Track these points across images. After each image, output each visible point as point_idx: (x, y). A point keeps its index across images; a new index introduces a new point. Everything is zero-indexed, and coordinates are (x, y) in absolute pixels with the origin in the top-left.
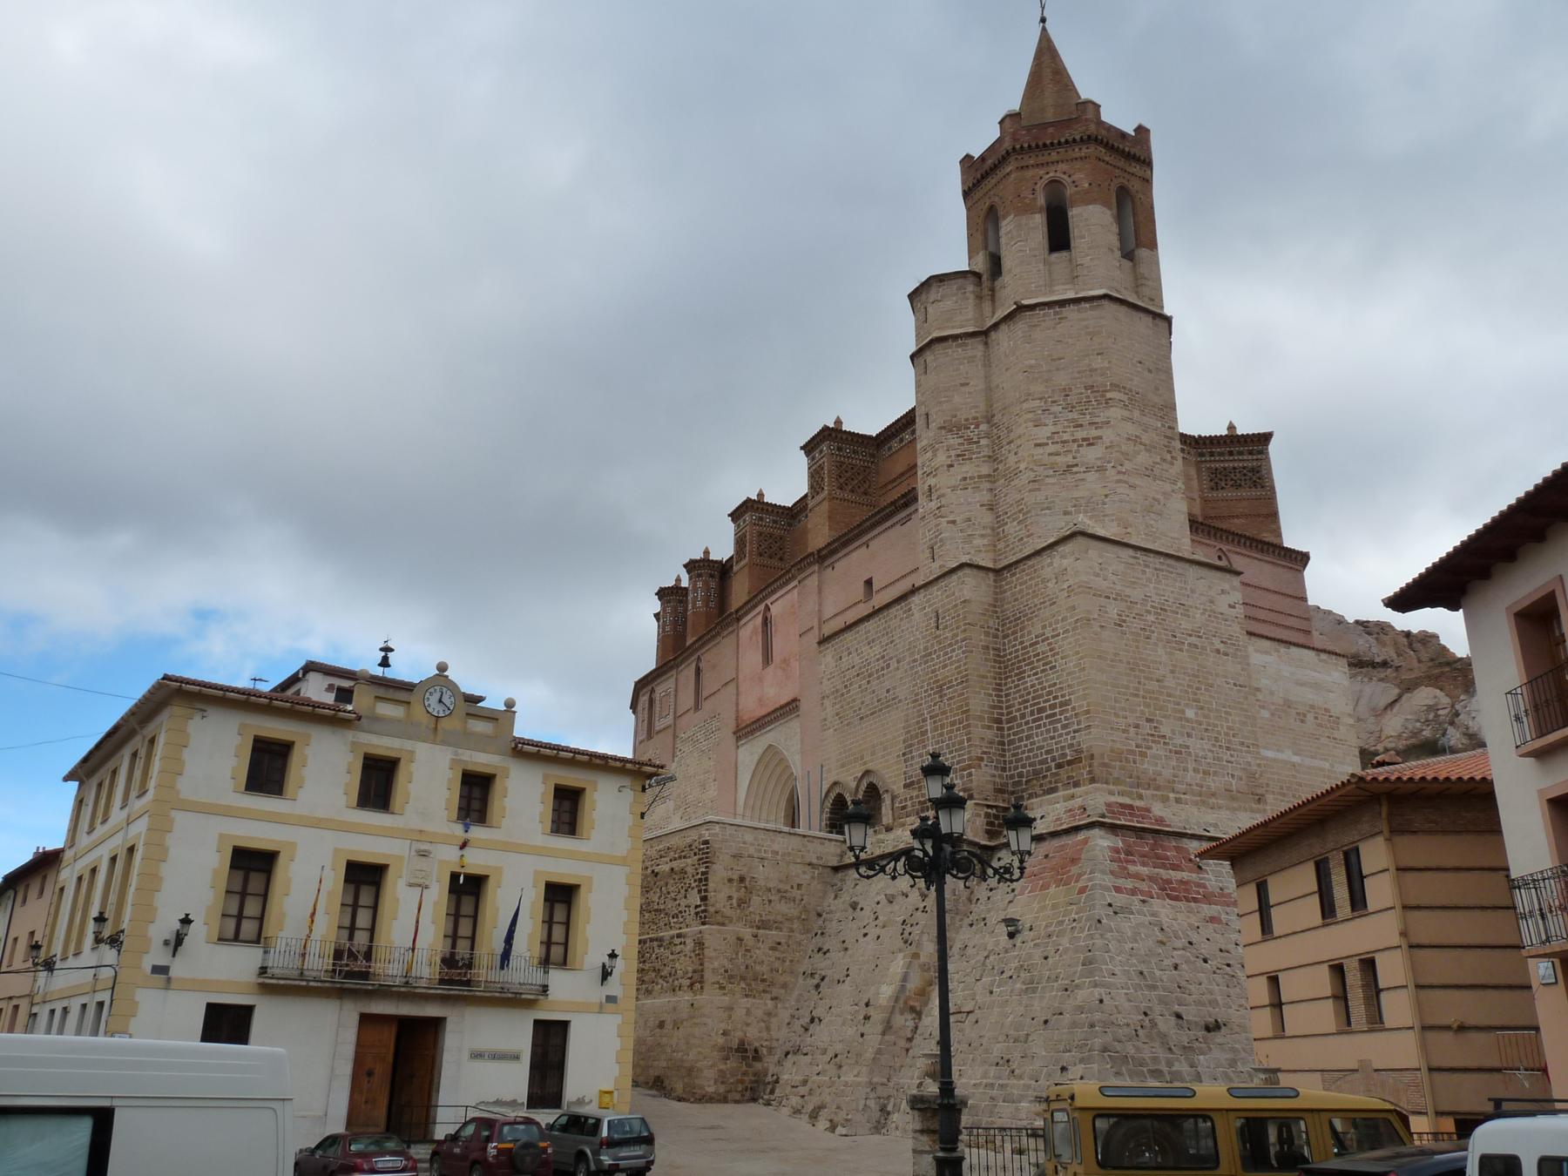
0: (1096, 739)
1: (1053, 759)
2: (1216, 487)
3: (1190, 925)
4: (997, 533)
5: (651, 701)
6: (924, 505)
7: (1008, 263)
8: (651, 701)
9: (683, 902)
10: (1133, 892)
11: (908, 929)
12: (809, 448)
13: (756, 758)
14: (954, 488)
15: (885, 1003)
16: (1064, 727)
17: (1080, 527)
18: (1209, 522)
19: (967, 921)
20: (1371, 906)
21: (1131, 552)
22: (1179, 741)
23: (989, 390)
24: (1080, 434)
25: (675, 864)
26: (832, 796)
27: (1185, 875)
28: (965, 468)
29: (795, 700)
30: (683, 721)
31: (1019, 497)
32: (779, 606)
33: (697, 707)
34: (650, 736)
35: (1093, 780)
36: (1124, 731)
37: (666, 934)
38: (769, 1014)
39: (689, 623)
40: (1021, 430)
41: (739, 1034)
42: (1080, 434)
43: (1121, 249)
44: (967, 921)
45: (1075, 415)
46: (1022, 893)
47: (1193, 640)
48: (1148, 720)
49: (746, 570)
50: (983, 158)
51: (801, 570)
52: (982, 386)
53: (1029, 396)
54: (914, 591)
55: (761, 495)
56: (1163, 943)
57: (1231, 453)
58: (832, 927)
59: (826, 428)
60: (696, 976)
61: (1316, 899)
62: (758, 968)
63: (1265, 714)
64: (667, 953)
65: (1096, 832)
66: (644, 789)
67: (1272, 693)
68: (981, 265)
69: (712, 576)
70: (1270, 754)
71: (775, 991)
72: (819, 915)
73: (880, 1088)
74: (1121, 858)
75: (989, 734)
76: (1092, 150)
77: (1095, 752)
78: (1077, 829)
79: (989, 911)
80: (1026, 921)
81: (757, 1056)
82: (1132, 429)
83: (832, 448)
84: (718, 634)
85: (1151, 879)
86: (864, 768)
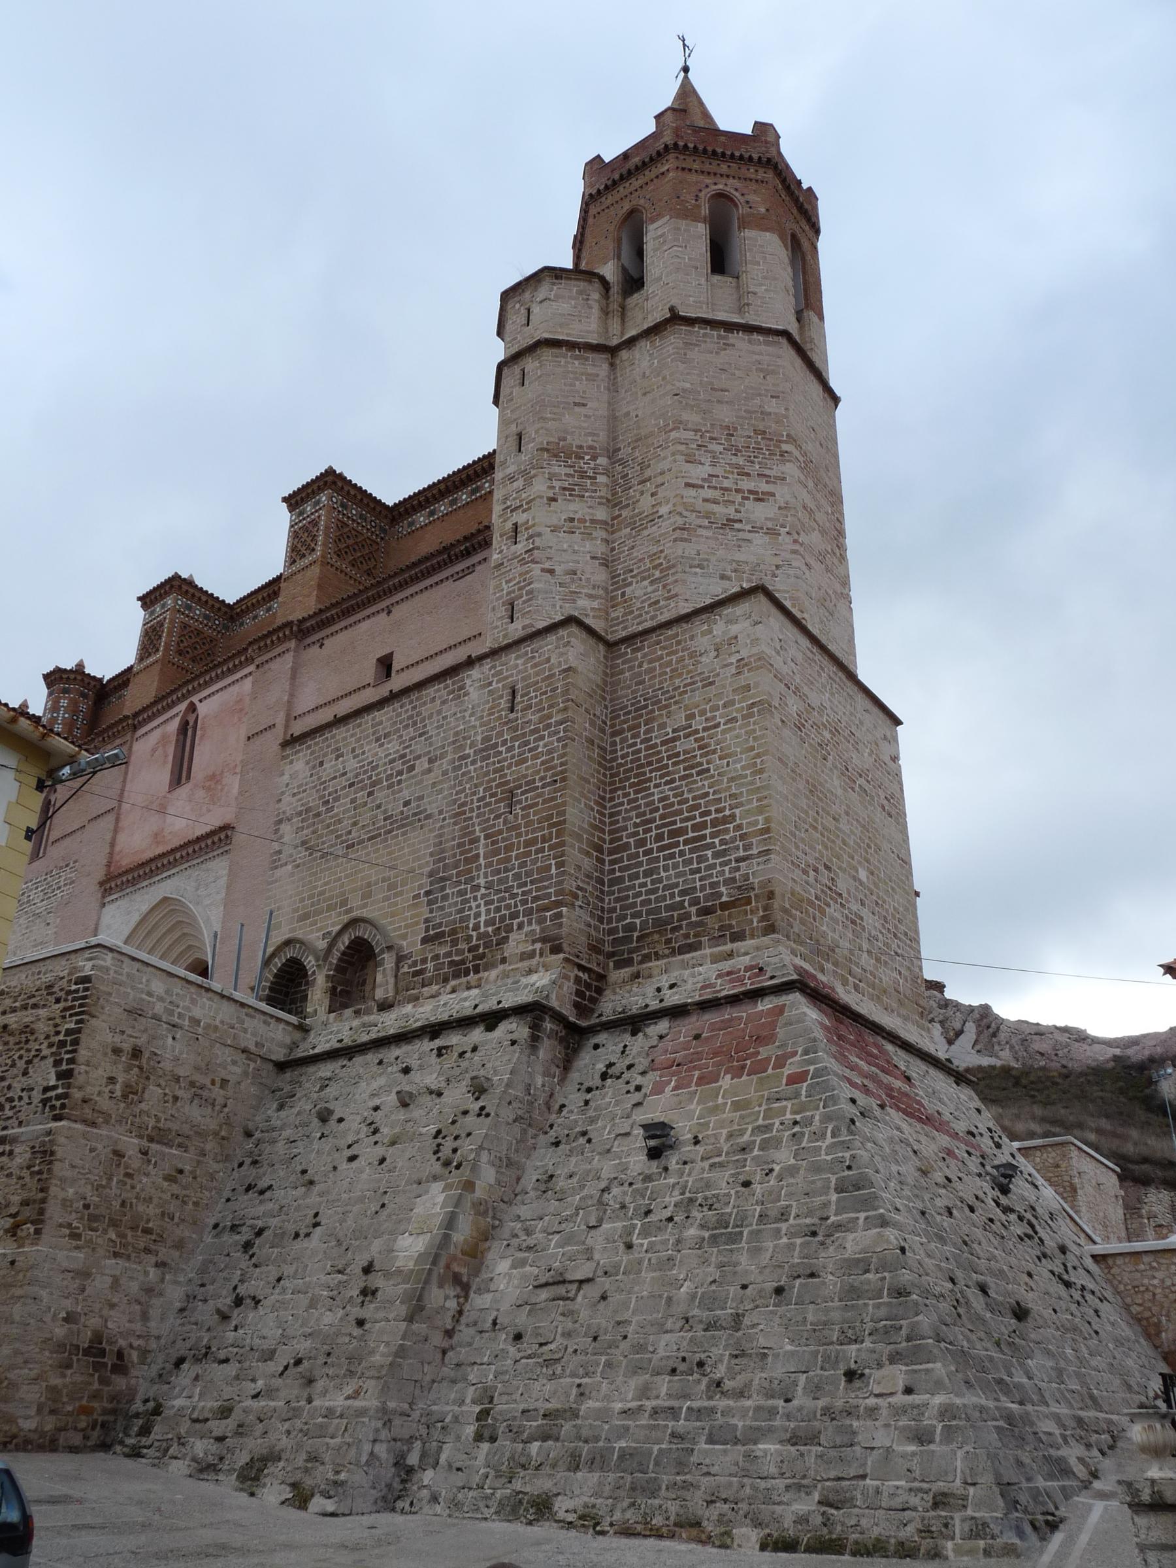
0: (780, 872)
6: (500, 550)
11: (449, 1144)
12: (294, 501)
13: (136, 918)
14: (555, 529)
15: (411, 1265)
16: (717, 855)
24: (746, 484)
29: (225, 828)
35: (771, 929)
38: (149, 1291)
40: (664, 465)
41: (94, 1322)
42: (746, 484)
49: (157, 667)
52: (603, 412)
53: (679, 424)
54: (470, 662)
60: (27, 1212)
62: (141, 1208)
69: (83, 695)
71: (164, 1253)
72: (249, 1134)
73: (397, 1421)
77: (778, 891)
78: (757, 994)
79: (592, 1121)
80: (683, 1129)
81: (121, 1366)
82: (804, 495)
86: (346, 918)
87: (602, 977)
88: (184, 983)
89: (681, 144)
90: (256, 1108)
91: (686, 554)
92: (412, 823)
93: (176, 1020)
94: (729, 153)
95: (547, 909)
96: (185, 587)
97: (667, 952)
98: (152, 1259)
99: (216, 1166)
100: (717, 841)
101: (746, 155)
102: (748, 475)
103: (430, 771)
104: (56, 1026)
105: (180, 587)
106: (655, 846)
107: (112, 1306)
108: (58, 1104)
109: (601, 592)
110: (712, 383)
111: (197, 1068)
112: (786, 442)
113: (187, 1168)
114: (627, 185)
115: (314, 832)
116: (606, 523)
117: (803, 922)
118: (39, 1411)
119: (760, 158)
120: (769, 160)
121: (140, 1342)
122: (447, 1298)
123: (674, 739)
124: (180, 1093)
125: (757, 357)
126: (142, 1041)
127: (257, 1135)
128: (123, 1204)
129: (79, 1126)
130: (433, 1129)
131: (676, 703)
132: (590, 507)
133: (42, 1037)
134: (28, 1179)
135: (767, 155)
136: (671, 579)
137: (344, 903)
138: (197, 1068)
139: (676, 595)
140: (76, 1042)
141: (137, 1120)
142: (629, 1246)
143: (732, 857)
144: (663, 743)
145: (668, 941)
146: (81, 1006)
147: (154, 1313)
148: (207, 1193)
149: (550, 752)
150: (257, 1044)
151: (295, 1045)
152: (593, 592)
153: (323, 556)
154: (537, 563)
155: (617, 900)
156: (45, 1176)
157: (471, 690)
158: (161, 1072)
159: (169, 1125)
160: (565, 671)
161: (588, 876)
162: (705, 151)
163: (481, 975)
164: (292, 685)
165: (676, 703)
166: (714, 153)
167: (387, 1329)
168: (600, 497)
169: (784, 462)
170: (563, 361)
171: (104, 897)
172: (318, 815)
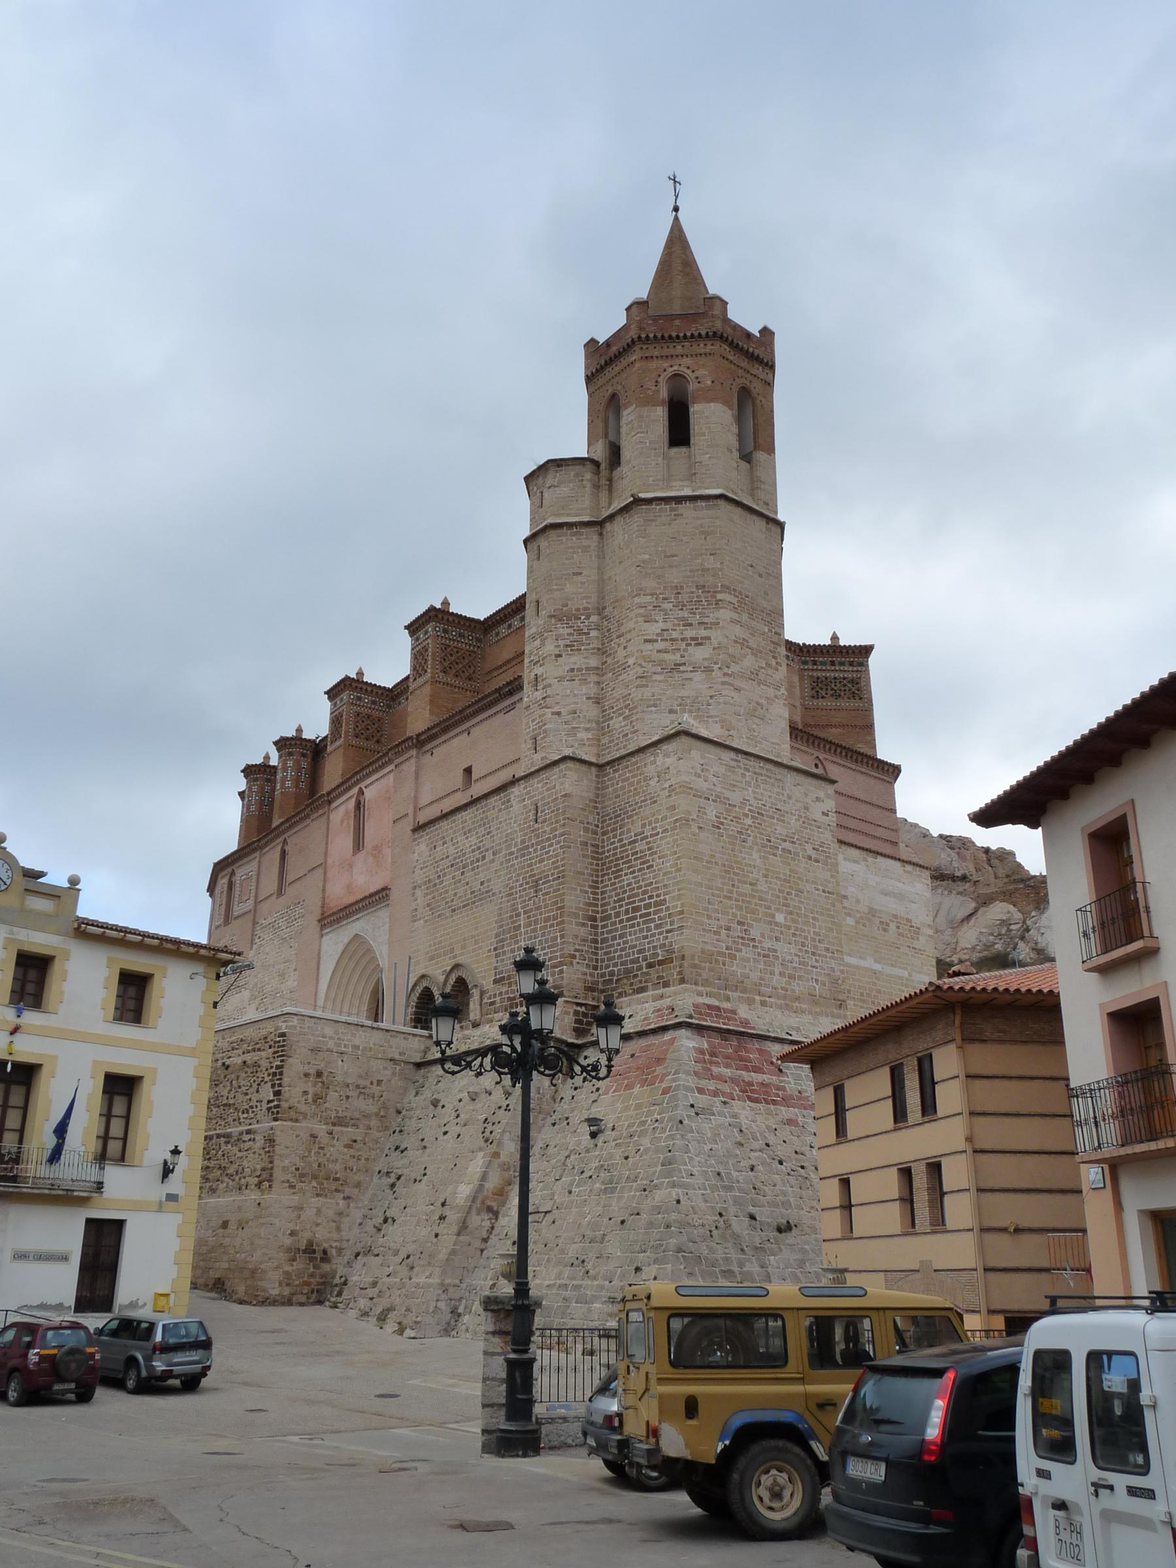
1: (645, 959)
3: (768, 1127)
4: (601, 727)
5: (231, 885)
6: (529, 694)
7: (626, 453)
8: (231, 885)
9: (255, 1097)
10: (715, 1093)
13: (341, 948)
14: (561, 679)
16: (657, 927)
17: (684, 727)
19: (550, 1120)
21: (732, 755)
22: (768, 944)
23: (601, 582)
25: (247, 1057)
26: (419, 989)
28: (573, 659)
29: (385, 889)
30: (264, 907)
32: (374, 789)
33: (280, 892)
34: (227, 921)
35: (682, 981)
36: (717, 933)
37: (234, 1130)
38: (340, 1214)
39: (277, 805)
40: (631, 625)
41: (307, 1235)
42: (690, 633)
43: (739, 450)
44: (550, 1120)
46: (606, 1093)
47: (787, 845)
48: (739, 923)
49: (341, 750)
50: (608, 344)
53: (641, 591)
54: (514, 782)
58: (412, 1124)
65: (683, 1032)
66: (218, 977)
67: (858, 901)
68: (600, 453)
69: (304, 755)
71: (348, 1191)
72: (399, 1112)
73: (451, 1290)
74: (706, 1059)
76: (717, 347)
78: (664, 1029)
79: (573, 1110)
80: (609, 1120)
81: (325, 1257)
82: (738, 631)
84: (307, 816)
86: (453, 962)
89: (643, 336)
90: (404, 1094)
94: (682, 335)
95: (556, 967)
96: (354, 685)
98: (341, 1195)
99: (379, 1135)
101: (696, 334)
102: (690, 625)
103: (493, 861)
107: (318, 1225)
109: (594, 725)
110: (664, 552)
111: (360, 1077)
112: (720, 592)
113: (359, 1138)
116: (597, 668)
118: (280, 1284)
120: (715, 333)
121: (337, 1244)
122: (483, 1220)
123: (635, 842)
125: (700, 522)
126: (322, 1066)
127: (404, 1112)
128: (319, 1166)
130: (483, 1117)
135: (714, 329)
136: (635, 717)
137: (452, 950)
138: (360, 1077)
140: (281, 1074)
142: (570, 1192)
144: (630, 843)
145: (631, 984)
147: (344, 1226)
149: (556, 856)
150: (400, 1054)
155: (606, 953)
157: (514, 803)
159: (345, 1114)
160: (565, 796)
161: (584, 940)
162: (663, 337)
164: (416, 783)
166: (670, 337)
167: (448, 1239)
169: (718, 609)
170: (564, 539)
172: (435, 885)
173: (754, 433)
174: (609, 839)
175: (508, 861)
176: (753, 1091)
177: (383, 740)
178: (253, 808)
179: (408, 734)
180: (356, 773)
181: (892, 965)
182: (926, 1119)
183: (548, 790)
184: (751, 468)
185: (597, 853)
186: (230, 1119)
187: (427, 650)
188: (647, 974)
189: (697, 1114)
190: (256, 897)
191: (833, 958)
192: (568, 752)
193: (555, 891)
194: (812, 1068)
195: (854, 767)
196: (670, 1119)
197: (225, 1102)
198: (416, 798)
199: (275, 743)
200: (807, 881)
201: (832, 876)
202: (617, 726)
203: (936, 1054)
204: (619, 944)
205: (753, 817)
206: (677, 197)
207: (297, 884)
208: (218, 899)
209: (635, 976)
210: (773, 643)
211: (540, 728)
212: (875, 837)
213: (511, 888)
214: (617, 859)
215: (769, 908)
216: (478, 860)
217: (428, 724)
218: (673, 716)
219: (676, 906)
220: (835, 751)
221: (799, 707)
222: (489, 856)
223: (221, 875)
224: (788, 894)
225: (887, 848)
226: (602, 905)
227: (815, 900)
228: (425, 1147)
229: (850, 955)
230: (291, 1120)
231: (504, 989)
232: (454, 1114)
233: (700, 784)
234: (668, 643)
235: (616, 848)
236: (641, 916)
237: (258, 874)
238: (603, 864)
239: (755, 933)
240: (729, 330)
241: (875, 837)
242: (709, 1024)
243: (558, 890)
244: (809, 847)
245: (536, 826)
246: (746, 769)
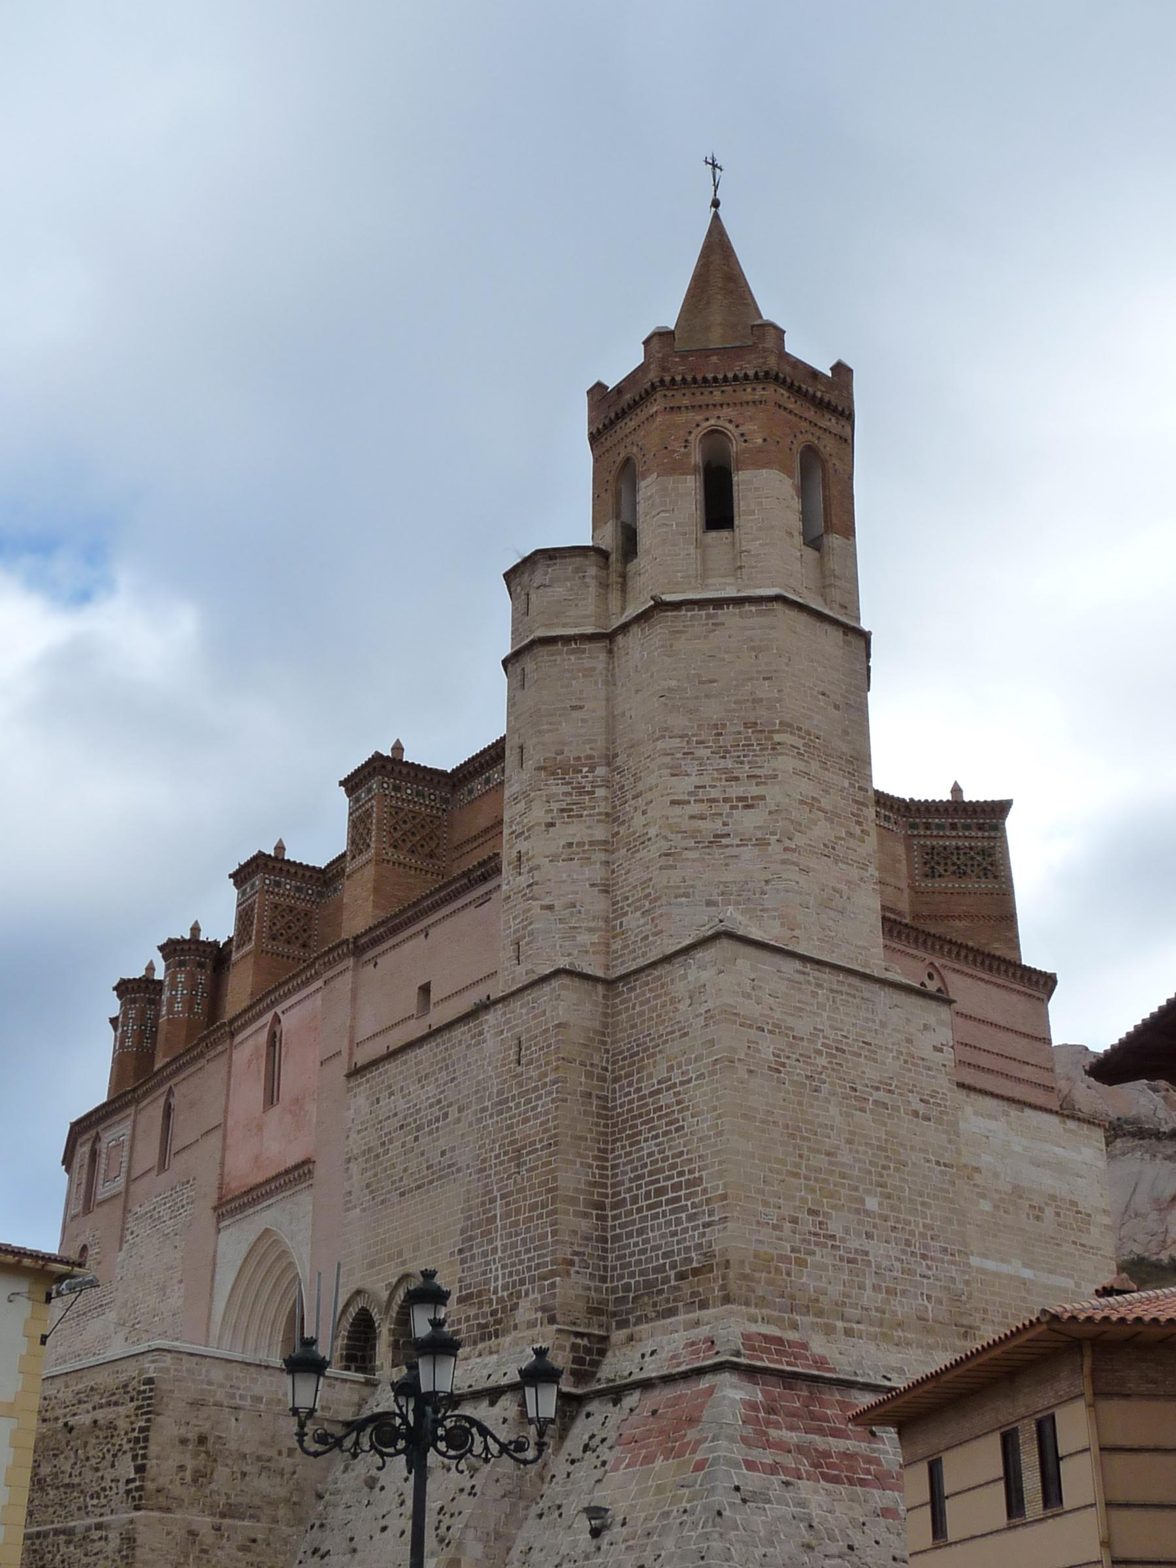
0: (736, 1239)
1: (673, 1266)
2: (931, 874)
3: (852, 1521)
4: (611, 926)
5: (94, 1154)
6: (509, 880)
7: (646, 540)
8: (94, 1154)
9: (109, 1474)
10: (773, 1469)
13: (244, 1249)
14: (553, 859)
16: (691, 1218)
17: (728, 926)
18: (916, 924)
19: (535, 1510)
20: (1068, 1502)
21: (798, 965)
22: (854, 1243)
23: (611, 721)
25: (100, 1415)
26: (353, 1311)
27: (850, 1445)
28: (572, 829)
29: (307, 1162)
30: (139, 1188)
31: (646, 876)
32: (296, 1014)
33: (162, 1166)
34: (87, 1209)
35: (727, 1300)
36: (775, 1227)
37: (79, 1523)
39: (161, 1038)
40: (652, 780)
42: (735, 791)
43: (804, 534)
44: (535, 1510)
45: (729, 763)
46: (615, 1469)
47: (881, 1095)
48: (811, 1212)
49: (251, 959)
50: (619, 389)
51: (329, 965)
53: (666, 732)
55: (280, 848)
56: (809, 1547)
57: (954, 827)
58: (337, 1515)
59: (377, 757)
61: (1001, 1485)
63: (986, 1206)
64: (79, 1553)
65: (726, 1377)
66: (49, 1299)
67: (996, 1175)
68: (609, 540)
69: (201, 965)
70: (990, 1265)
72: (320, 1497)
74: (759, 1418)
75: (584, 1225)
76: (772, 393)
77: (733, 1257)
78: (700, 1372)
79: (567, 1494)
80: (618, 1510)
82: (806, 788)
83: (384, 783)
84: (201, 1055)
85: (800, 1449)
86: (401, 1270)
87: (605, 1339)
88: (242, 1366)
89: (667, 379)
91: (672, 883)
92: (447, 1175)
93: (238, 1402)
94: (720, 376)
97: (654, 1315)
100: (689, 1203)
102: (737, 779)
103: (459, 1120)
104: (132, 1423)
105: (266, 865)
106: (644, 1203)
108: (137, 1495)
109: (601, 924)
110: (699, 676)
111: (262, 1443)
112: (778, 732)
113: (260, 1537)
114: (622, 424)
115: (375, 1175)
116: (606, 842)
117: (770, 1282)
119: (756, 374)
120: (767, 373)
123: (659, 1091)
124: (247, 1469)
126: (206, 1427)
127: (327, 1497)
129: (156, 1514)
131: (660, 1052)
132: (589, 827)
133: (123, 1433)
134: (119, 1562)
135: (766, 368)
136: (658, 912)
137: (400, 1254)
138: (262, 1443)
139: (661, 932)
140: (146, 1439)
141: (208, 1500)
143: (700, 1222)
145: (655, 1305)
146: (149, 1405)
148: (282, 1557)
149: (547, 1113)
151: (363, 1401)
152: (592, 925)
153: (377, 854)
154: (537, 899)
155: (619, 1258)
156: (130, 1560)
157: (487, 1035)
158: (227, 1453)
159: (239, 1499)
160: (558, 1026)
163: (499, 1340)
165: (660, 1052)
166: (705, 380)
168: (599, 814)
170: (558, 658)
171: (218, 1222)
172: (377, 1156)
173: (825, 509)
174: (622, 1088)
175: (480, 1120)
176: (831, 1466)
177: (313, 943)
178: (129, 1042)
179: (344, 936)
180: (270, 993)
181: (1050, 1272)
182: (1049, 1512)
183: (535, 1017)
184: (822, 557)
185: (605, 1108)
186: (74, 1507)
187: (370, 816)
188: (677, 1288)
189: (744, 1501)
190: (129, 1173)
191: (953, 1263)
192: (563, 962)
193: (544, 1165)
194: (899, 1433)
195: (986, 977)
196: (705, 1508)
197: (67, 1481)
198: (352, 1027)
199: (161, 948)
200: (912, 1148)
201: (950, 1141)
202: (633, 925)
203: (1061, 1415)
204: (636, 1244)
205: (829, 1055)
206: (716, 187)
207: (185, 1156)
208: (76, 1175)
209: (661, 1292)
210: (857, 802)
211: (524, 928)
212: (1019, 1080)
213: (484, 1161)
214: (634, 1118)
215: (856, 1189)
216: (437, 1120)
217: (371, 922)
218: (712, 910)
219: (716, 1188)
220: (958, 954)
221: (907, 891)
222: (453, 1113)
223: (80, 1141)
224: (884, 1167)
225: (1039, 1097)
226: (614, 1186)
227: (924, 1177)
228: (354, 1550)
229: (985, 1256)
230: (160, 1509)
231: (472, 1312)
232: (397, 1500)
233: (750, 1008)
234: (705, 806)
235: (631, 1102)
236: (668, 1202)
237: (133, 1137)
238: (615, 1125)
239: (835, 1227)
240: (788, 369)
241: (1019, 1080)
242: (767, 1364)
243: (550, 1163)
244: (914, 1099)
245: (519, 1069)
246: (819, 986)
